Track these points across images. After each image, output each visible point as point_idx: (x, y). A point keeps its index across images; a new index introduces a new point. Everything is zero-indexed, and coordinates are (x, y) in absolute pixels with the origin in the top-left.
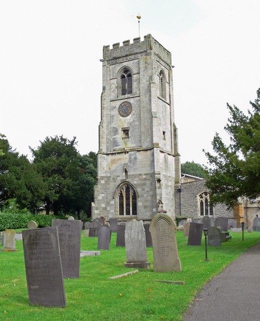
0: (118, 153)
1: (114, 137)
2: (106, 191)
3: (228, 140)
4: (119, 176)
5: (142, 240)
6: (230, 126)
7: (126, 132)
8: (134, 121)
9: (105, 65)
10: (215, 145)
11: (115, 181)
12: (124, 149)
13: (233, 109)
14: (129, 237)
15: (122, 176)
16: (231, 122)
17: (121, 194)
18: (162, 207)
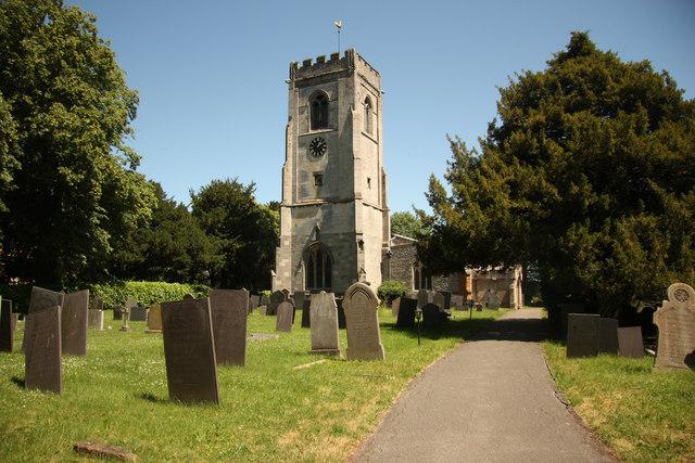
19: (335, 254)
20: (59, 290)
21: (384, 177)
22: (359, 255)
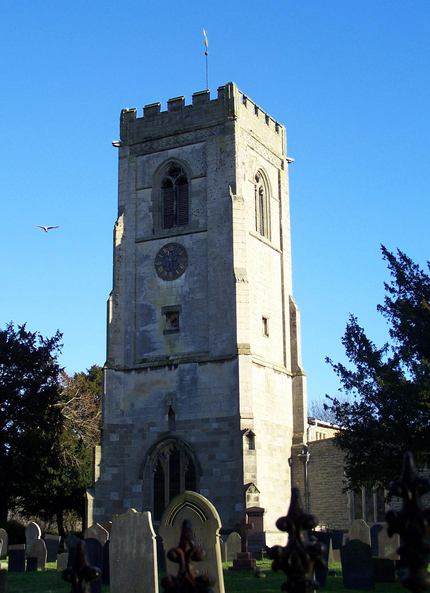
0: (153, 368)
1: (145, 328)
2: (123, 462)
3: (381, 333)
4: (153, 424)
5: (131, 553)
6: (394, 300)
7: (173, 317)
8: (192, 291)
9: (125, 157)
10: (350, 347)
11: (144, 437)
12: (168, 358)
13: (398, 260)
14: (117, 551)
15: (162, 423)
16: (392, 291)
17: (159, 468)
18: (257, 499)
19: (202, 457)
20: (108, 424)
21: (293, 314)
22: (247, 460)
